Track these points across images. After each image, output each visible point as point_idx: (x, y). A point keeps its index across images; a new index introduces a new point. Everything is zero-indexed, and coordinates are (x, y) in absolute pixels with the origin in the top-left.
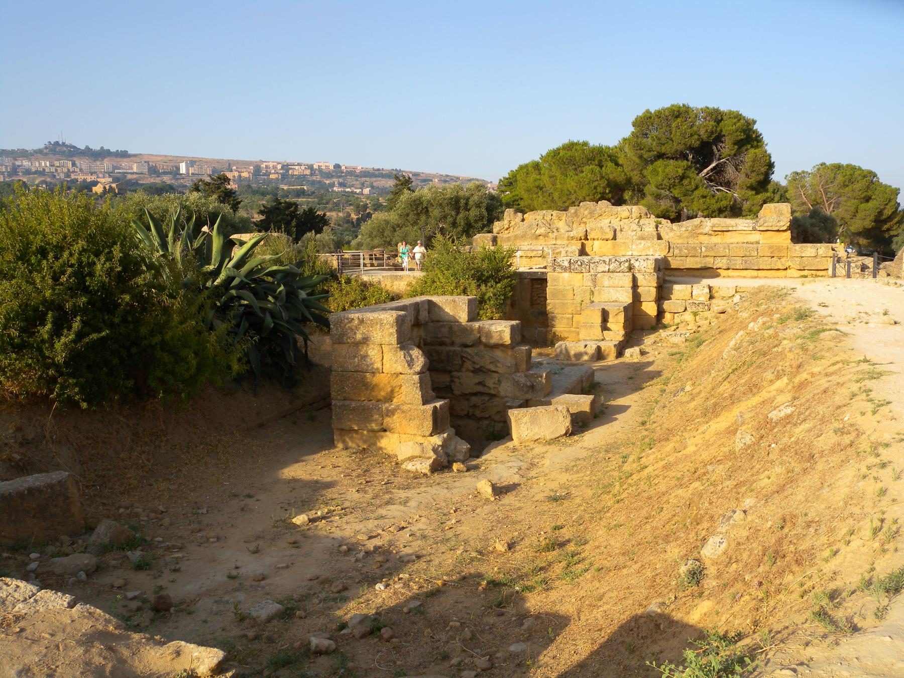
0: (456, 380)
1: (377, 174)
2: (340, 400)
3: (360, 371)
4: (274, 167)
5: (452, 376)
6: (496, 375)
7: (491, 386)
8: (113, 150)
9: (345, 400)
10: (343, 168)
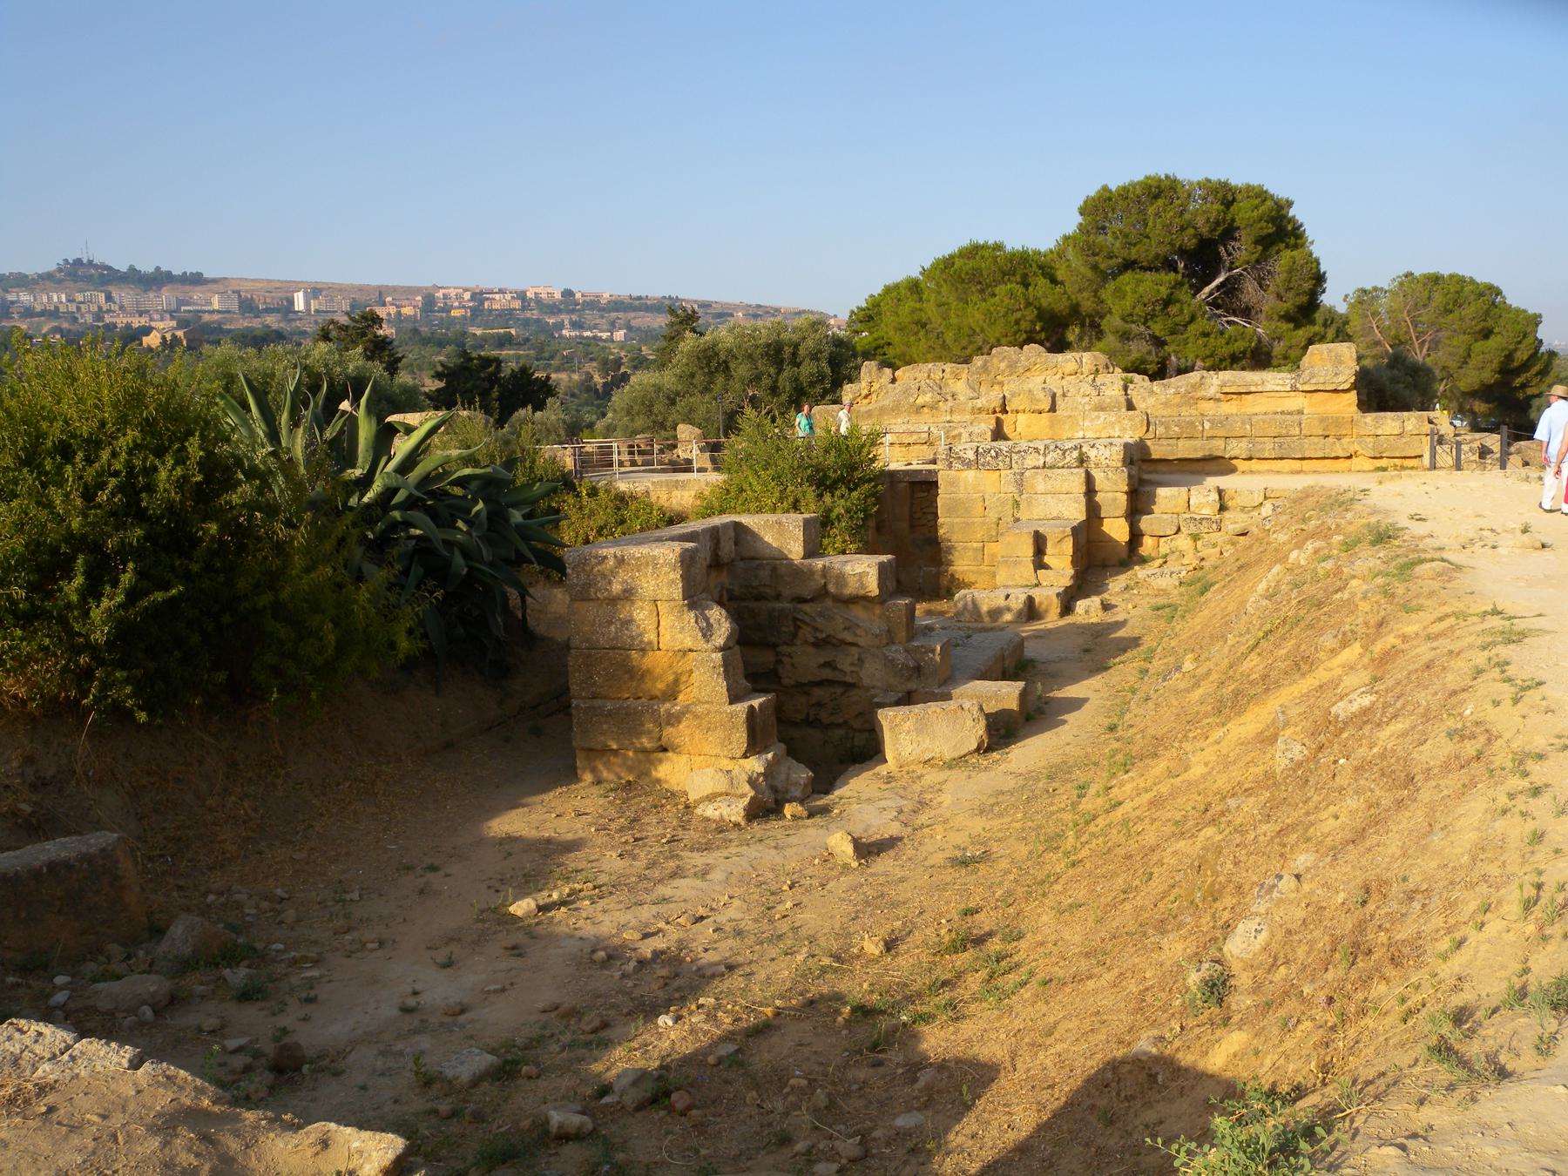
0: (785, 659)
1: (638, 305)
2: (585, 698)
3: (619, 648)
4: (459, 297)
5: (777, 654)
6: (854, 650)
7: (848, 668)
8: (177, 272)
9: (594, 698)
10: (578, 296)
